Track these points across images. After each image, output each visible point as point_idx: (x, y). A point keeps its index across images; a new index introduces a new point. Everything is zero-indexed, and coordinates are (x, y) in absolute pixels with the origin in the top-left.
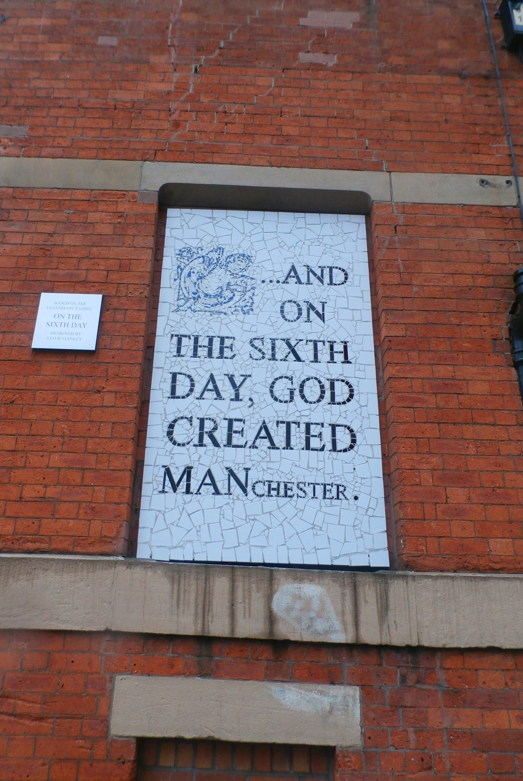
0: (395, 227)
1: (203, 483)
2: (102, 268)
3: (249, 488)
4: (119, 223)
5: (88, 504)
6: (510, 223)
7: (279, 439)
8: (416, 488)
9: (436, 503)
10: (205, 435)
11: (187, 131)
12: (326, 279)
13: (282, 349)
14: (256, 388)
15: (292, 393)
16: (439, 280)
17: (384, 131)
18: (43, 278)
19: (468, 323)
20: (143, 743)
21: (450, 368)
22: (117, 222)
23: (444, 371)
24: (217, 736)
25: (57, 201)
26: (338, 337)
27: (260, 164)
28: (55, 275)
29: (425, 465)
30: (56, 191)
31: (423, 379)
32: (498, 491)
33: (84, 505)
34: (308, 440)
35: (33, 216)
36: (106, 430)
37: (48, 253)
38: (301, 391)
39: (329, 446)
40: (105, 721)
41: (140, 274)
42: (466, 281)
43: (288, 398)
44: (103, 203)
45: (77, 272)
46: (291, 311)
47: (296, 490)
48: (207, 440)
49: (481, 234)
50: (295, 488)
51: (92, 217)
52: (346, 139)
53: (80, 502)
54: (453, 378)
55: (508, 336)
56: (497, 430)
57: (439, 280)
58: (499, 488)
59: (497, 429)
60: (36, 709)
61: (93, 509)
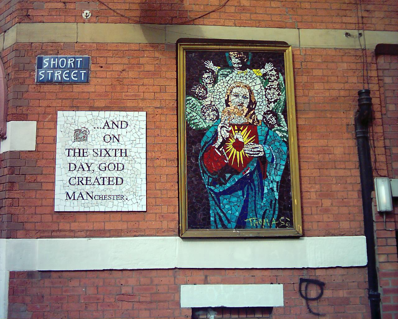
0: (301, 63)
1: (79, 197)
2: (151, 91)
3: (93, 197)
4: (157, 64)
5: (160, 214)
6: (360, 59)
7: (101, 181)
8: (308, 200)
9: (317, 207)
10: (80, 182)
11: (188, 4)
12: (120, 126)
13: (104, 152)
14: (94, 167)
15: (105, 168)
16: (322, 93)
17: (296, 3)
18: (120, 98)
19: (335, 117)
20: (194, 310)
21: (326, 141)
22: (156, 63)
23: (322, 142)
24: (225, 306)
25: (122, 51)
26: (123, 147)
27: (230, 25)
28: (127, 96)
29: (313, 189)
30: (120, 44)
31: (313, 147)
32: (345, 200)
33: (158, 215)
34: (87, 183)
35: (110, 61)
36: (164, 178)
37: (121, 83)
38: (108, 167)
39: (115, 184)
40: (178, 303)
41: (171, 94)
42: (335, 93)
43: (104, 170)
44: (147, 51)
45: (138, 93)
46: (107, 138)
47: (108, 198)
48: (80, 183)
49: (345, 66)
50: (108, 197)
51: (142, 61)
52: (275, 8)
53: (156, 213)
54: (327, 146)
55: (354, 123)
56: (347, 171)
57: (322, 93)
58: (345, 198)
59: (346, 171)
60: (148, 299)
61: (162, 216)
